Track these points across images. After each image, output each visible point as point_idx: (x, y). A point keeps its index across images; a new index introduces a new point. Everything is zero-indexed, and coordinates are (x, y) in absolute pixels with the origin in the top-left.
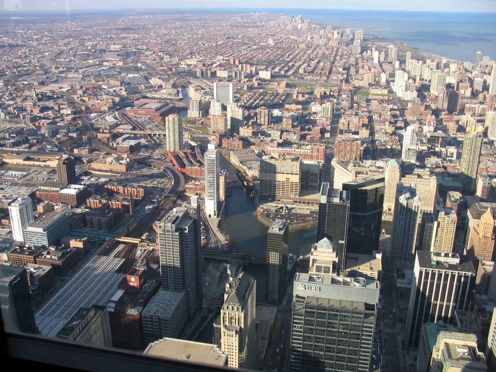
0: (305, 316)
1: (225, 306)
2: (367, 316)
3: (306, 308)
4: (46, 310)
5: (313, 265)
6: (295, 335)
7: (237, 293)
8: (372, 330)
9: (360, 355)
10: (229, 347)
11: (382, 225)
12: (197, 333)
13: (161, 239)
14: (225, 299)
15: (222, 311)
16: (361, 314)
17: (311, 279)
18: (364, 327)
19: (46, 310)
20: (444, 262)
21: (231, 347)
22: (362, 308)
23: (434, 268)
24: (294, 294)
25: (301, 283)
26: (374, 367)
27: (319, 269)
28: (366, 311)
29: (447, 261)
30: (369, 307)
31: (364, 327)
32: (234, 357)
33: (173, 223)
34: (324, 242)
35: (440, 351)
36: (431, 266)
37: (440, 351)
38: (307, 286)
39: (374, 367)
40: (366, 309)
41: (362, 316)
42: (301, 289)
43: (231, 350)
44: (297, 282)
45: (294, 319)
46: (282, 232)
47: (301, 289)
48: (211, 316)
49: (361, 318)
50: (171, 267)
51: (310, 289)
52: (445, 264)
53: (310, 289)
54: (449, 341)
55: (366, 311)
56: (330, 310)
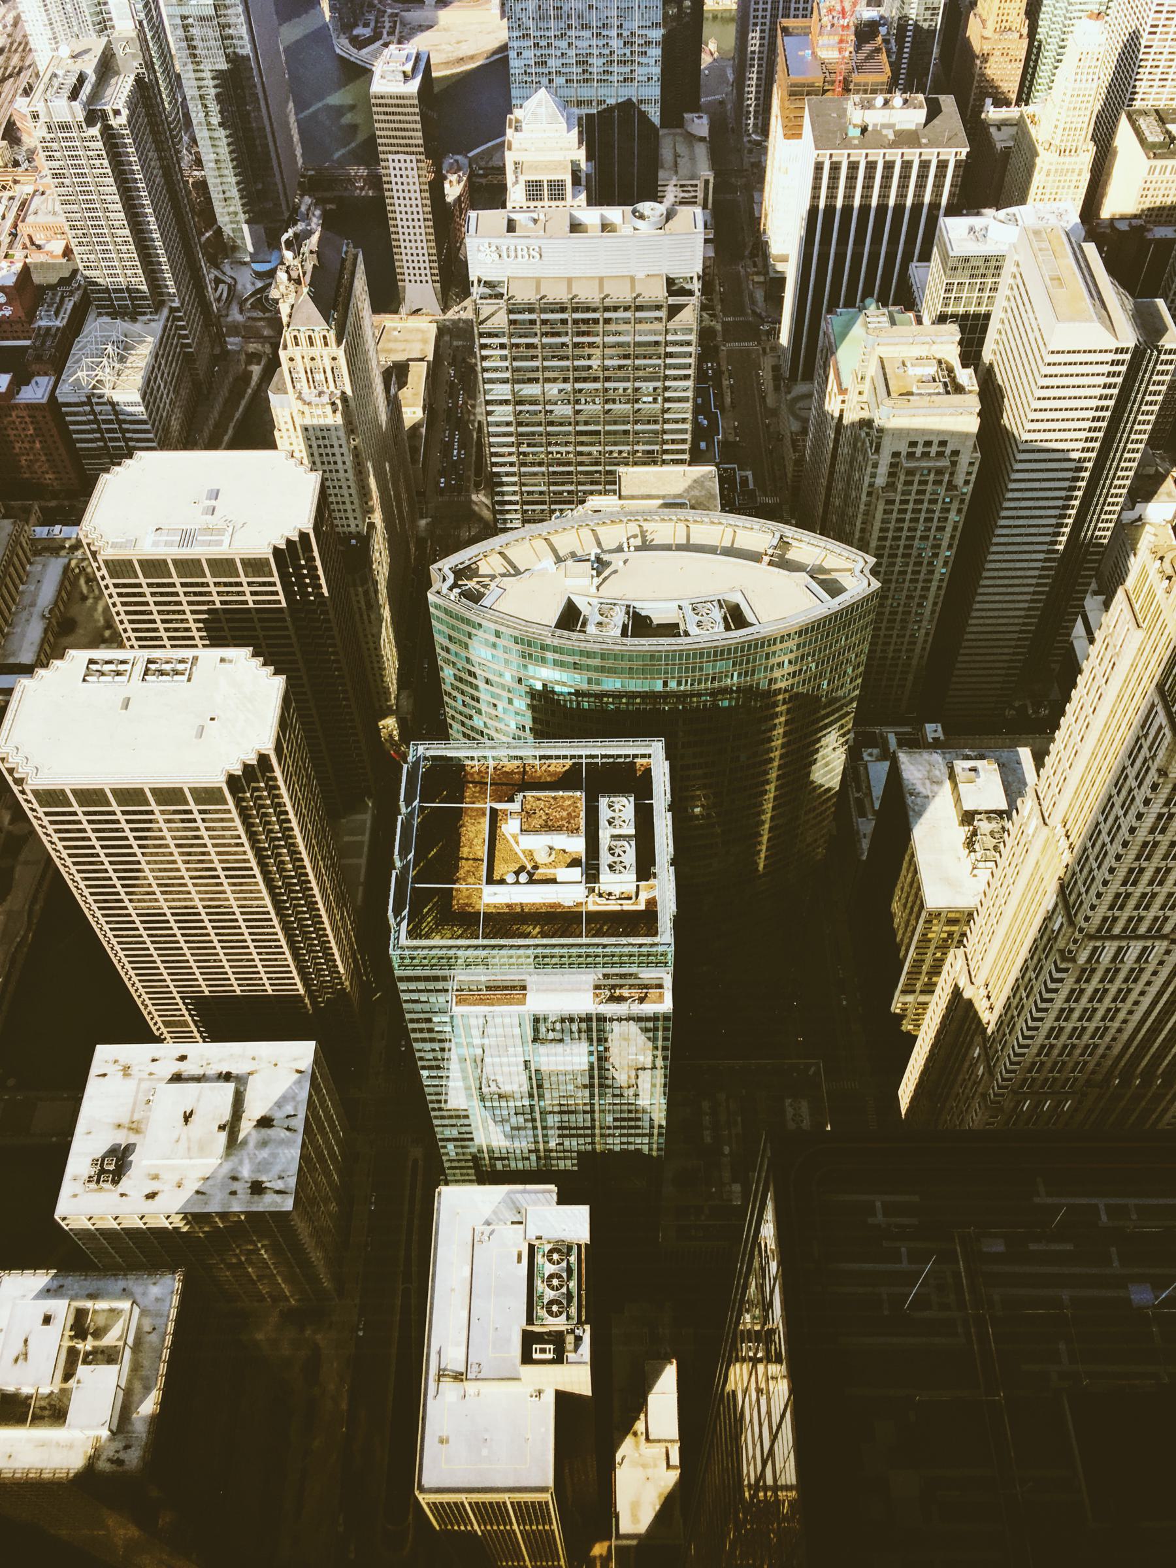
0: (511, 335)
1: (287, 335)
2: (674, 310)
3: (510, 312)
4: (101, 888)
5: (517, 182)
6: (496, 455)
7: (316, 298)
8: (691, 349)
9: (665, 442)
10: (322, 450)
11: (708, 29)
12: (232, 425)
13: (49, 158)
14: (285, 320)
15: (281, 353)
16: (658, 308)
17: (511, 227)
18: (664, 432)
19: (101, 888)
20: (884, 126)
21: (329, 450)
22: (658, 292)
23: (856, 147)
24: (473, 277)
25: (487, 240)
26: (703, 445)
27: (534, 191)
28: (671, 301)
29: (892, 121)
30: (674, 287)
31: (664, 432)
32: (342, 474)
33: (74, 95)
34: (539, 104)
35: (868, 381)
36: (846, 143)
37: (868, 381)
38: (504, 248)
39: (703, 445)
40: (671, 293)
41: (663, 314)
42: (489, 260)
43: (329, 450)
44: (477, 240)
45: (485, 370)
46: (414, 86)
47: (489, 260)
48: (256, 370)
49: (659, 319)
50: (121, 291)
51: (512, 254)
52: (884, 132)
53: (512, 254)
54: (885, 352)
55: (671, 301)
56: (576, 310)
